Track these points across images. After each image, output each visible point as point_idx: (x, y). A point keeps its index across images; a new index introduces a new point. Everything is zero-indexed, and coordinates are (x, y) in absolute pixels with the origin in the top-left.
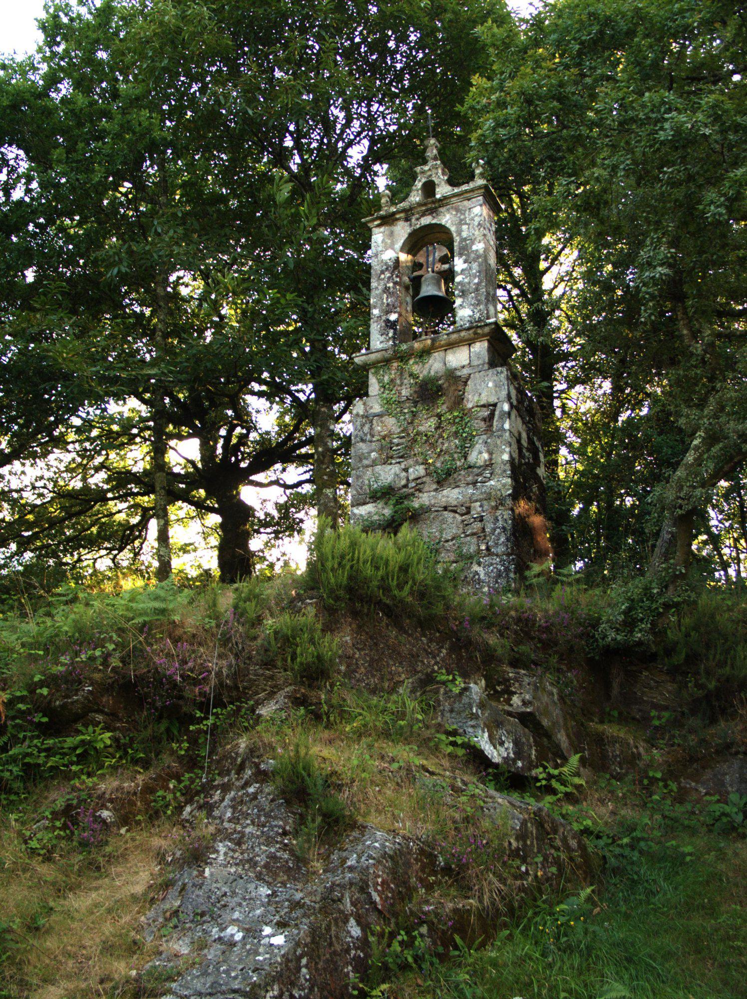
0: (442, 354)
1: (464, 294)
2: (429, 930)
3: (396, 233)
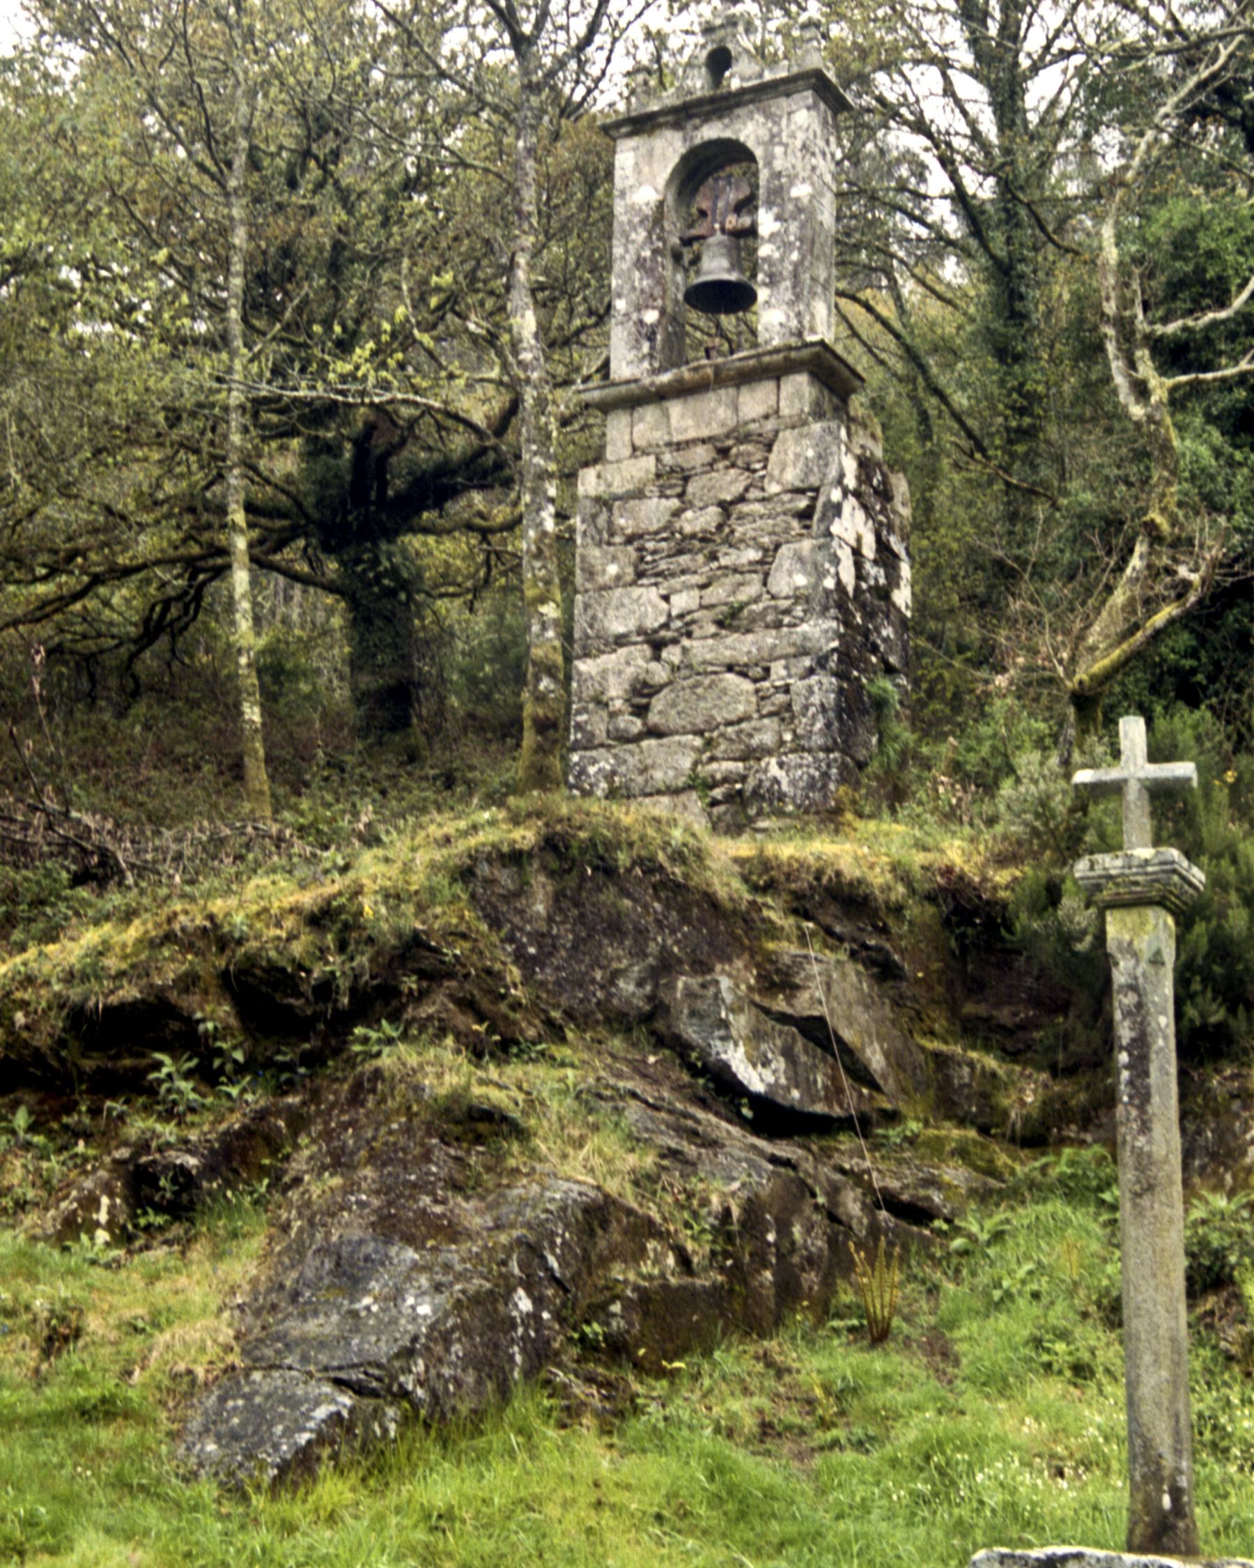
0: (732, 391)
1: (773, 281)
2: (624, 1308)
3: (658, 152)
